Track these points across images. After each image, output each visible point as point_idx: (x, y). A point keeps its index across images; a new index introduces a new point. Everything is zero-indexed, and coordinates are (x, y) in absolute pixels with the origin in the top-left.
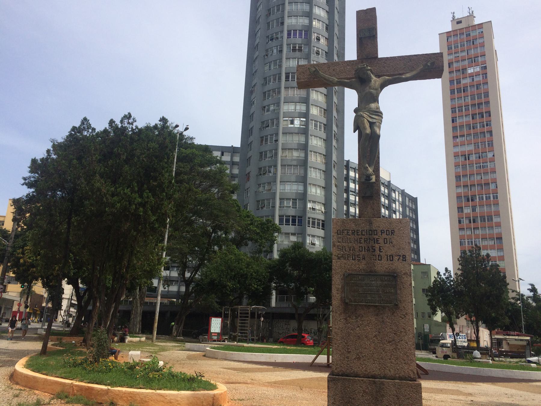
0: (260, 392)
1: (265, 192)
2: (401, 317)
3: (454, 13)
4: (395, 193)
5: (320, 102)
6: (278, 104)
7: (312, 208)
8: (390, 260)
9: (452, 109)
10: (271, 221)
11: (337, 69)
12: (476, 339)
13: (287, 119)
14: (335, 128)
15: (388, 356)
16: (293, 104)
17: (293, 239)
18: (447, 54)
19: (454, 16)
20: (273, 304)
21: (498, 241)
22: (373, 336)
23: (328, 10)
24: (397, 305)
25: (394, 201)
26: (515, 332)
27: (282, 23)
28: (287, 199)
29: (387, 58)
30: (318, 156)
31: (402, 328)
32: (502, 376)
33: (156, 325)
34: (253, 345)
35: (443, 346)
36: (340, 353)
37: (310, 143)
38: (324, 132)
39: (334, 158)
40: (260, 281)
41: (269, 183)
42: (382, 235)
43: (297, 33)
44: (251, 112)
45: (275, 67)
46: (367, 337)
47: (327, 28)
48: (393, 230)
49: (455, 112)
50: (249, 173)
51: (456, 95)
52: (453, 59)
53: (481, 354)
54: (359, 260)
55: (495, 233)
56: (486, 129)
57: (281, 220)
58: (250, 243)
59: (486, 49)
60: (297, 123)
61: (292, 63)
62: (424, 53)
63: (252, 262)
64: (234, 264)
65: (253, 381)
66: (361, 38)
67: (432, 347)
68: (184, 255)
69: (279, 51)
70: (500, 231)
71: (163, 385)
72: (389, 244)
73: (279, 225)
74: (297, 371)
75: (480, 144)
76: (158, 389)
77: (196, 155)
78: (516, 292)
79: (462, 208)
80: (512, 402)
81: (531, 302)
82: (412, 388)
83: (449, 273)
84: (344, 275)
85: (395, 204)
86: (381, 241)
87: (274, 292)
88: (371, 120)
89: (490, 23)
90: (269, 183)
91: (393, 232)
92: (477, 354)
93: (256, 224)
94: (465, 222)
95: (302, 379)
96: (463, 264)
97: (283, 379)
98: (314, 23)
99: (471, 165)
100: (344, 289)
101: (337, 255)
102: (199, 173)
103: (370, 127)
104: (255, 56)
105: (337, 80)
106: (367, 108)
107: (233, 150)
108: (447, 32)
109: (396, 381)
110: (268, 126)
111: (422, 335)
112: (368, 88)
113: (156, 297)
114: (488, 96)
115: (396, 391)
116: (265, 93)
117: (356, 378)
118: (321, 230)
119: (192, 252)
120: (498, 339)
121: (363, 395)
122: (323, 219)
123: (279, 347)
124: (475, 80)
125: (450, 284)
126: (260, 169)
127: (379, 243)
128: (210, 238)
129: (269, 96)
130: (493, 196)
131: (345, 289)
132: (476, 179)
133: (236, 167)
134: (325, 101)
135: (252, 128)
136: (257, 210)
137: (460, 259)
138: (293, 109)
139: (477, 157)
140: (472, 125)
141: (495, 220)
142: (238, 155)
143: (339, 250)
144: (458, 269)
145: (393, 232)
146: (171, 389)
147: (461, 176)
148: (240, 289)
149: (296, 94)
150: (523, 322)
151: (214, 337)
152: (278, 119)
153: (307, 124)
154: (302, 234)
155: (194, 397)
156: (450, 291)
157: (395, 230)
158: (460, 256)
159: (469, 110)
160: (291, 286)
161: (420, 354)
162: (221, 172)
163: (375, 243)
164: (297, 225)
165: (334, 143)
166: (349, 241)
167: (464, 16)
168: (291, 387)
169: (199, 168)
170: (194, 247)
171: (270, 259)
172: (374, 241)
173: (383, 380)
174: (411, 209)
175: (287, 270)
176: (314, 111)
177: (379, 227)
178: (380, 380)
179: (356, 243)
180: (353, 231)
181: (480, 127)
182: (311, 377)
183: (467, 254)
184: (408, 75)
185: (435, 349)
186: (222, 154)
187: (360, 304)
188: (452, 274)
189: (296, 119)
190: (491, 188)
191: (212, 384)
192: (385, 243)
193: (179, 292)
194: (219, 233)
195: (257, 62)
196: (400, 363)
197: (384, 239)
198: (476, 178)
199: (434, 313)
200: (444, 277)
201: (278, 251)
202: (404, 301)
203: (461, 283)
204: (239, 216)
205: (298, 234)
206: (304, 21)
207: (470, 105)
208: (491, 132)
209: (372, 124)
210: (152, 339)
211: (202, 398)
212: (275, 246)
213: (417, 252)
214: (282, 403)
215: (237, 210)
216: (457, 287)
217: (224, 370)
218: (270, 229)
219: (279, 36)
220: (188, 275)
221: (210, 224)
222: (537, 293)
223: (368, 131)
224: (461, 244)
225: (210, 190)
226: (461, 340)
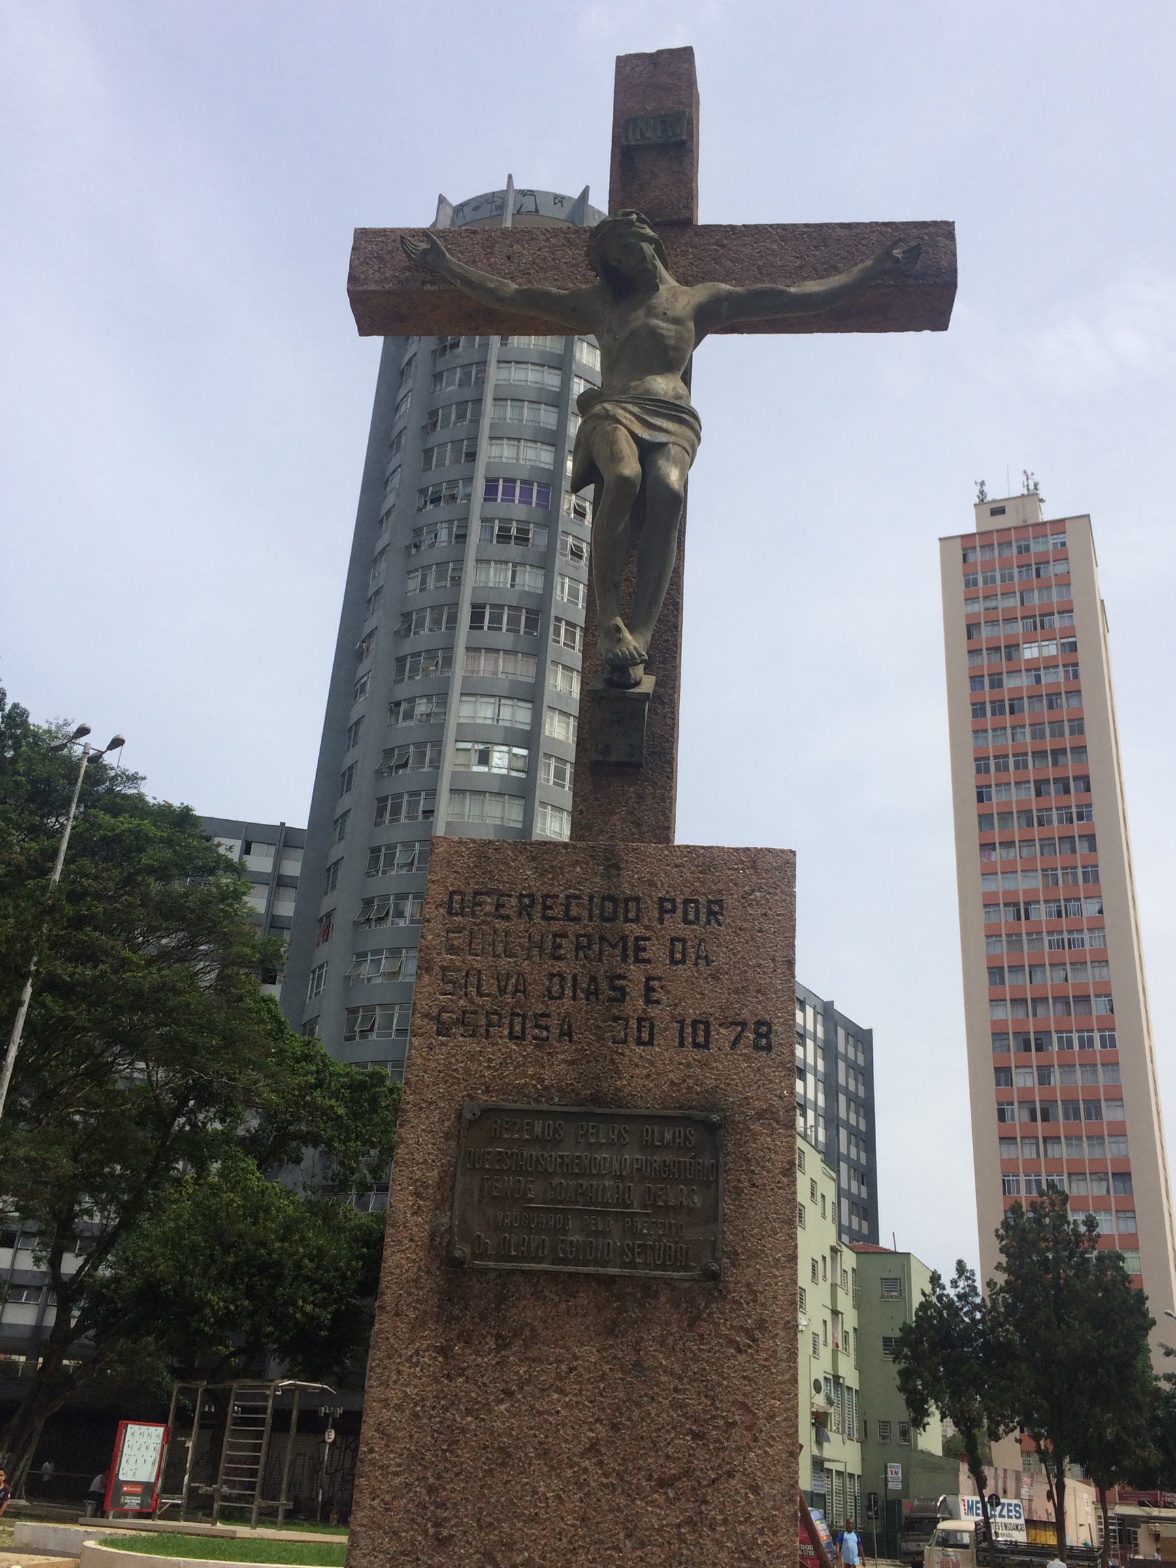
1: (378, 981)
2: (731, 1342)
3: (982, 484)
4: (803, 1010)
6: (442, 697)
8: (696, 1045)
9: (976, 759)
11: (521, 255)
13: (468, 745)
16: (492, 700)
19: (982, 492)
21: (1120, 1185)
22: (580, 1449)
24: (714, 1276)
27: (472, 456)
29: (732, 228)
31: (734, 1403)
34: (274, 1531)
36: (393, 1548)
40: (327, 1288)
42: (661, 921)
43: (514, 488)
44: (355, 716)
45: (439, 584)
46: (546, 1452)
48: (719, 902)
49: (987, 771)
50: (329, 915)
51: (987, 693)
54: (541, 1043)
55: (1109, 1156)
56: (1076, 828)
61: (495, 577)
63: (303, 1219)
64: (241, 1226)
67: (912, 1546)
68: (67, 1190)
69: (457, 536)
70: (1123, 1153)
72: (696, 964)
75: (1060, 872)
77: (149, 840)
79: (1007, 1070)
84: (460, 1116)
85: (804, 1045)
86: (656, 950)
88: (645, 434)
89: (1087, 519)
91: (716, 908)
94: (1019, 1116)
96: (1012, 1251)
99: (1035, 934)
100: (452, 1188)
101: (435, 1011)
103: (642, 460)
104: (379, 548)
106: (635, 388)
108: (963, 537)
110: (405, 765)
111: (880, 1504)
112: (641, 312)
114: (1081, 732)
116: (401, 661)
120: (1123, 1519)
124: (1043, 682)
125: (973, 1319)
126: (368, 902)
127: (648, 961)
129: (414, 670)
131: (459, 1188)
132: (1049, 982)
135: (351, 768)
136: (347, 1039)
137: (1001, 1232)
138: (490, 716)
139: (1050, 912)
140: (1035, 813)
141: (1109, 1114)
142: (299, 853)
143: (449, 987)
144: (997, 1268)
147: (1006, 969)
148: (251, 1315)
149: (500, 669)
152: (438, 744)
156: (970, 1341)
157: (729, 901)
158: (1002, 1223)
159: (1026, 766)
163: (625, 958)
166: (500, 948)
167: (1012, 495)
172: (625, 949)
177: (652, 884)
179: (537, 959)
180: (526, 901)
181: (1060, 821)
183: (1023, 1214)
185: (921, 1553)
186: (247, 850)
187: (526, 1266)
188: (978, 1284)
189: (496, 748)
190: (1094, 1013)
192: (674, 962)
193: (38, 1328)
195: (383, 565)
197: (673, 940)
198: (1050, 979)
199: (919, 1420)
200: (951, 1292)
202: (749, 1258)
203: (1007, 1315)
207: (1030, 754)
208: (1091, 839)
209: (648, 452)
216: (993, 1330)
223: (631, 467)
224: (1006, 1187)
226: (1006, 1520)
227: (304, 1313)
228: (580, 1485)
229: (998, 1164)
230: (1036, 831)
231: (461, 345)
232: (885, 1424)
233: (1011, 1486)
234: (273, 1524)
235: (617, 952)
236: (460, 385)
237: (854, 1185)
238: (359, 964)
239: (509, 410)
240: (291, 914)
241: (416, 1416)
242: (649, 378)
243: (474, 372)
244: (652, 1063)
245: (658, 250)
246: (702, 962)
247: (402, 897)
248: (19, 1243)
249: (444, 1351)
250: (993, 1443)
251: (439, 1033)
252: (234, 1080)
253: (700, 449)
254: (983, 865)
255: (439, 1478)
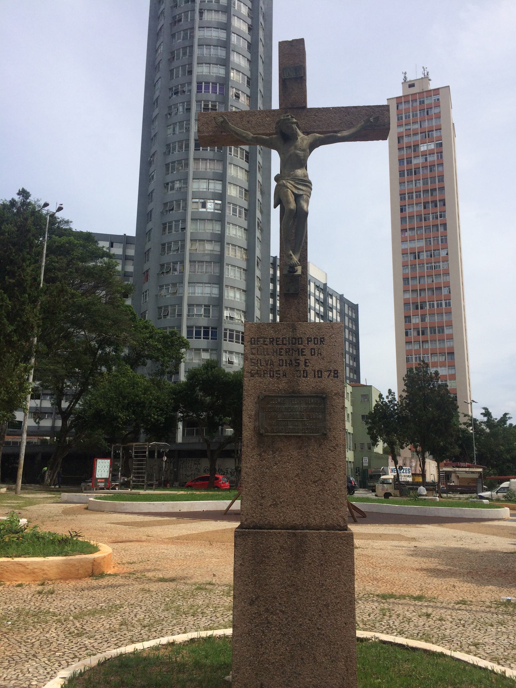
0: (157, 552)
2: (330, 450)
3: (405, 73)
4: (332, 298)
5: (240, 180)
6: (185, 180)
7: (230, 317)
8: (319, 377)
9: (400, 195)
10: (176, 334)
12: (421, 473)
13: (197, 200)
14: (258, 214)
15: (313, 500)
16: (206, 181)
17: (206, 356)
18: (396, 125)
19: (405, 77)
20: (180, 439)
23: (250, 58)
24: (325, 435)
25: (331, 309)
26: (465, 463)
27: (190, 72)
28: (198, 305)
29: (319, 109)
30: (237, 250)
32: (450, 515)
33: (21, 471)
35: (384, 482)
37: (227, 234)
38: (245, 219)
39: (258, 253)
41: (174, 285)
43: (209, 86)
44: (150, 190)
45: (180, 131)
46: (286, 476)
47: (248, 83)
48: (323, 338)
50: (147, 271)
52: (403, 132)
53: (427, 490)
54: (278, 378)
55: (446, 347)
57: (190, 333)
58: (149, 362)
59: (443, 121)
60: (210, 206)
62: (366, 105)
65: (149, 538)
66: (285, 79)
67: (372, 484)
68: (59, 379)
70: (452, 345)
71: (23, 550)
73: (188, 338)
74: (208, 522)
75: (432, 239)
76: (16, 557)
78: (468, 416)
80: (462, 546)
81: (485, 428)
82: (341, 539)
83: (392, 395)
84: (259, 398)
85: (332, 312)
86: (307, 352)
87: (180, 425)
88: (296, 192)
90: (174, 285)
91: (322, 340)
92: (422, 490)
93: (157, 337)
94: (413, 334)
95: (213, 532)
97: (189, 532)
98: (232, 74)
99: (422, 264)
101: (250, 371)
102: (77, 270)
103: (296, 200)
104: (155, 114)
105: (252, 135)
107: (126, 240)
108: (397, 98)
109: (322, 531)
110: (172, 210)
112: (293, 148)
113: (21, 435)
114: (443, 181)
115: (322, 544)
116: (167, 165)
117: (272, 531)
118: (240, 344)
119: (71, 375)
120: (446, 472)
121: (279, 552)
122: (243, 331)
123: (186, 493)
124: (428, 160)
125: (394, 409)
126: (162, 266)
127: (305, 355)
128: (95, 356)
129: (173, 169)
130: (446, 303)
133: (131, 262)
134: (246, 178)
136: (159, 319)
137: (405, 378)
138: (205, 187)
141: (447, 331)
142: (133, 246)
143: (253, 364)
145: (322, 341)
146: (34, 555)
148: (135, 420)
150: (475, 452)
151: (100, 484)
152: (185, 200)
153: (223, 208)
154: (217, 350)
155: (65, 563)
157: (326, 338)
160: (202, 416)
161: (360, 493)
162: (110, 267)
163: (299, 355)
164: (210, 338)
165: (258, 234)
166: (266, 353)
168: (199, 542)
169: (79, 263)
170: (73, 368)
171: (175, 382)
172: (299, 352)
173: (305, 531)
174: (350, 318)
175: (197, 396)
176: (232, 192)
177: (305, 334)
178: (302, 531)
180: (272, 340)
181: (433, 218)
182: (224, 528)
184: (345, 133)
186: (112, 245)
187: (278, 434)
188: (397, 397)
189: (208, 201)
190: (443, 294)
191: (92, 546)
192: (312, 355)
193: (53, 427)
194: (108, 350)
195: (156, 123)
196: (327, 508)
197: (312, 349)
198: (427, 281)
199: (375, 443)
200: (386, 400)
201: (185, 372)
203: (406, 407)
204: (134, 327)
205: (212, 350)
206: (218, 71)
208: (445, 225)
209: (297, 197)
210: (15, 490)
211: (77, 565)
212: (182, 365)
213: (356, 371)
214: (185, 563)
215: (131, 319)
216: (401, 412)
217: (112, 525)
218: (176, 343)
219: (186, 89)
220: (65, 405)
221: (95, 338)
222: (491, 417)
223: (293, 205)
224: (408, 360)
225: (94, 293)
226: (405, 474)
227: (154, 419)
228: (295, 483)
229: (405, 352)
230: (423, 224)
231: (182, 20)
232: (362, 444)
233: (408, 462)
234: (151, 489)
235: (297, 353)
236: (183, 40)
237: (351, 362)
238: (161, 290)
239: (205, 51)
240: (133, 271)
241: (254, 470)
242: (296, 170)
243: (189, 33)
244: (307, 382)
245: (298, 126)
246: (319, 355)
247: (175, 263)
248: (42, 398)
249: (260, 455)
250: (401, 450)
251: (251, 376)
252: (119, 337)
253: (312, 192)
254: (402, 238)
255: (261, 483)
